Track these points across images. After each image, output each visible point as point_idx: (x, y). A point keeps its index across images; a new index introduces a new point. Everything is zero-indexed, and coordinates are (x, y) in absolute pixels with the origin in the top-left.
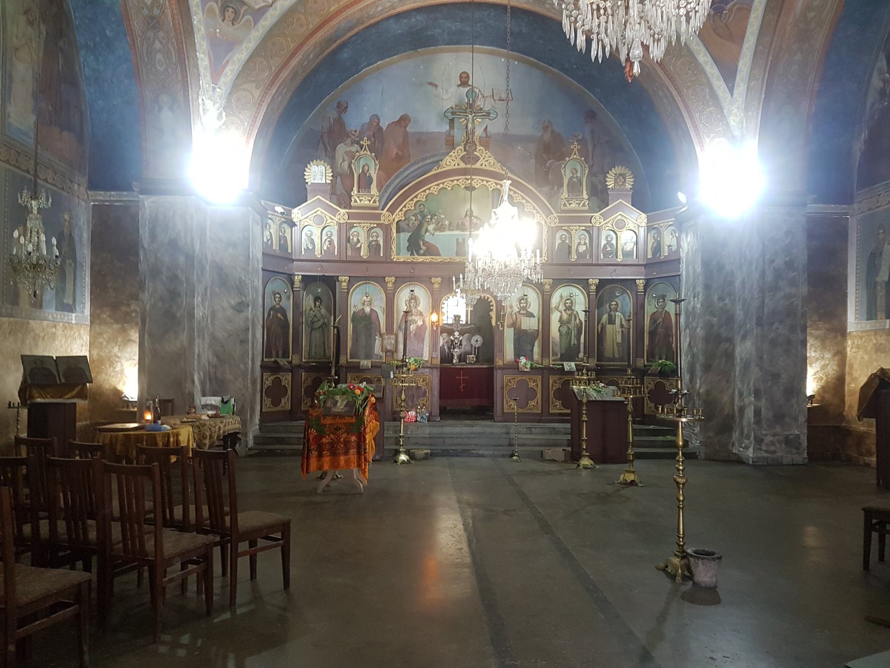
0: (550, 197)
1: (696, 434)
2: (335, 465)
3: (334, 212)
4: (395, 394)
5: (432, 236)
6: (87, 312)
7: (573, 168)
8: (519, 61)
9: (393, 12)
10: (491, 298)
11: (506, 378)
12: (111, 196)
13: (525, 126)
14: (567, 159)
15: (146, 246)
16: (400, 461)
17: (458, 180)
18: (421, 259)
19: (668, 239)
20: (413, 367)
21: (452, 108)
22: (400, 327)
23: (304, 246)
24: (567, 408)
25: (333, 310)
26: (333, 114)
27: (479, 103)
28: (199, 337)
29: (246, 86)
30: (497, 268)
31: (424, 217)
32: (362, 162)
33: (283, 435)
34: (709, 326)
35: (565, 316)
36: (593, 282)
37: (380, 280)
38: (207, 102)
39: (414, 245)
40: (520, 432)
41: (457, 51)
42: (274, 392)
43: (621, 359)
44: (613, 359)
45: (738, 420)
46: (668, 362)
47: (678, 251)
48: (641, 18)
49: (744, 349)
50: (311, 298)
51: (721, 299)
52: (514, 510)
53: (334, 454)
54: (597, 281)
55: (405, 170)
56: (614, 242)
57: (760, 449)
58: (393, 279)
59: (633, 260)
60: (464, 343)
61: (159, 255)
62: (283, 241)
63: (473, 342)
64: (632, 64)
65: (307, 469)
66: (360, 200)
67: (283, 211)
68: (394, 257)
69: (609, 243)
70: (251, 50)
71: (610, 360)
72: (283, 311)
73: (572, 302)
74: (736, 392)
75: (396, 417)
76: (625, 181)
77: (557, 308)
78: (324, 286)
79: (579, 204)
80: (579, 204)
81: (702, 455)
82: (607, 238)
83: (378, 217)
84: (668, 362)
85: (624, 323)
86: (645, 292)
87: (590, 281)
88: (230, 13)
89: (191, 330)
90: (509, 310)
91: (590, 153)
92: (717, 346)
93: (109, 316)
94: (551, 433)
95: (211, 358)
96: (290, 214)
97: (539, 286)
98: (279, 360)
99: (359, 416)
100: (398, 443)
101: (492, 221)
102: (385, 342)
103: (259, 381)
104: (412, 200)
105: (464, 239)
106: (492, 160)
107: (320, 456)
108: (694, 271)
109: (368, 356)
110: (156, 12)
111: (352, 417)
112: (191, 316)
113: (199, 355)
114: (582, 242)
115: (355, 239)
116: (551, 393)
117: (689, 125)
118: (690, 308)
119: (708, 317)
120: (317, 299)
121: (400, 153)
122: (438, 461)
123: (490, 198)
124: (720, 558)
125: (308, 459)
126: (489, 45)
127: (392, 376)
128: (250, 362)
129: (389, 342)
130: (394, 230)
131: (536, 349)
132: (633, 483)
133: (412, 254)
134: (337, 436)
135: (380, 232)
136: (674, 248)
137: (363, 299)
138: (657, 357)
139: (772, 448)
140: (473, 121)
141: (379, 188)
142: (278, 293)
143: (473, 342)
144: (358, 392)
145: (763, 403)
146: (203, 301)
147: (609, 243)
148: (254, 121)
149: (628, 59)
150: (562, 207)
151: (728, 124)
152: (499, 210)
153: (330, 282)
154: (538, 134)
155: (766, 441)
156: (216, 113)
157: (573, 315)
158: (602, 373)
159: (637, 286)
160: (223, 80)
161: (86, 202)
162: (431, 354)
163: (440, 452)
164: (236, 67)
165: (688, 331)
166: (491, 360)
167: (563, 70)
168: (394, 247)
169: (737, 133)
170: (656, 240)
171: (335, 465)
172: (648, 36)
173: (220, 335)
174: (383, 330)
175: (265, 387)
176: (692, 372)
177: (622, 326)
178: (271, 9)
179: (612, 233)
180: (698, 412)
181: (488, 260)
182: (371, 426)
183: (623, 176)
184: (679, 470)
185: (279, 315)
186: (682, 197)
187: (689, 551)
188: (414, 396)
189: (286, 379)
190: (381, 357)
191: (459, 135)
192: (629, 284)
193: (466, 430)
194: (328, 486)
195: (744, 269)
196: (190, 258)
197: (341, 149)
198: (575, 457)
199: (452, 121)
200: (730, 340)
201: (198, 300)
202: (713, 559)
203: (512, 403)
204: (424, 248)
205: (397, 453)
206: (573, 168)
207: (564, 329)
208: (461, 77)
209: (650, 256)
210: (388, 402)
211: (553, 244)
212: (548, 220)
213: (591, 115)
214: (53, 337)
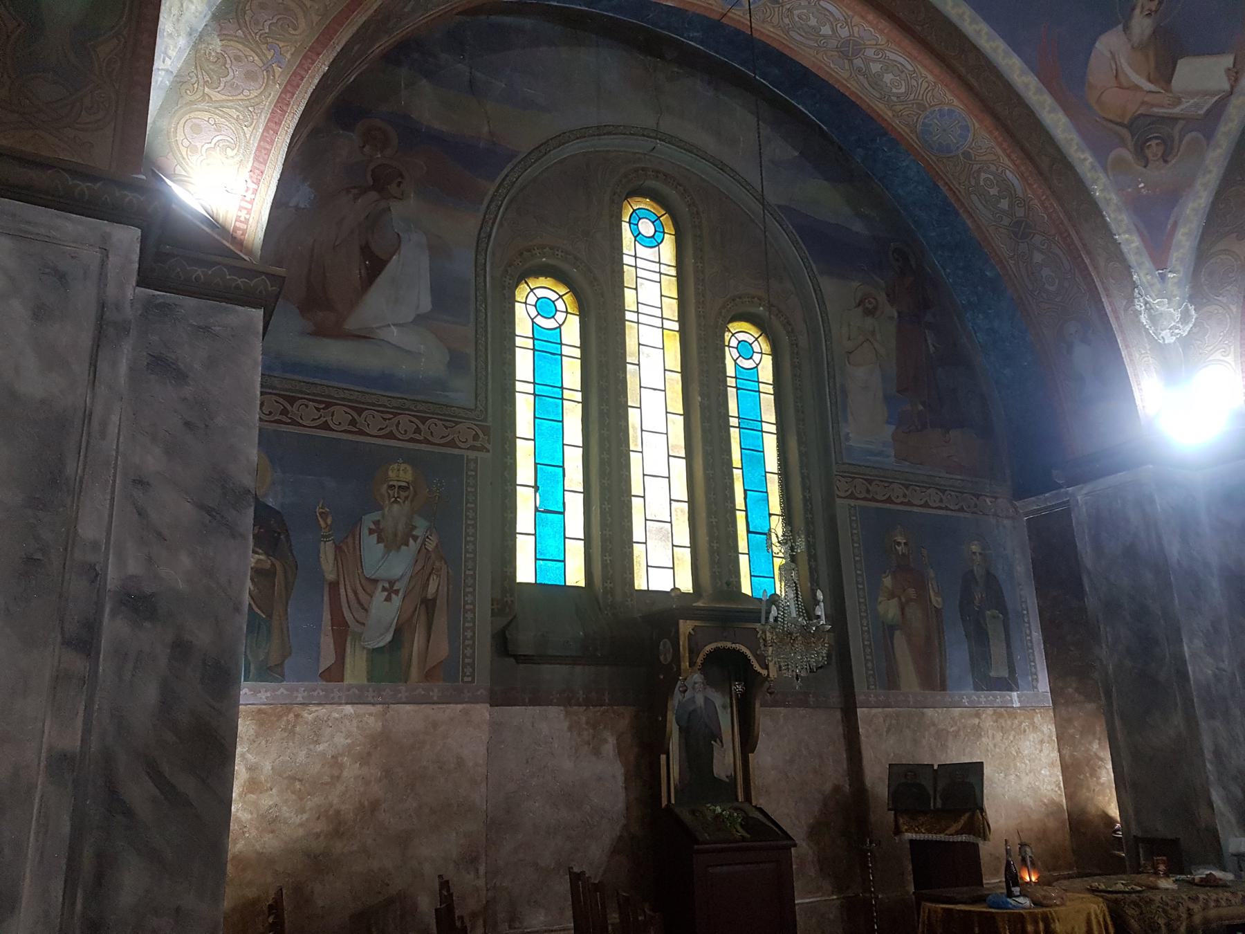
6: (1044, 685)
88: (1154, 148)
93: (1077, 690)
110: (1020, 213)
112: (1183, 676)
113: (1217, 753)
156: (1177, 315)
214: (977, 732)
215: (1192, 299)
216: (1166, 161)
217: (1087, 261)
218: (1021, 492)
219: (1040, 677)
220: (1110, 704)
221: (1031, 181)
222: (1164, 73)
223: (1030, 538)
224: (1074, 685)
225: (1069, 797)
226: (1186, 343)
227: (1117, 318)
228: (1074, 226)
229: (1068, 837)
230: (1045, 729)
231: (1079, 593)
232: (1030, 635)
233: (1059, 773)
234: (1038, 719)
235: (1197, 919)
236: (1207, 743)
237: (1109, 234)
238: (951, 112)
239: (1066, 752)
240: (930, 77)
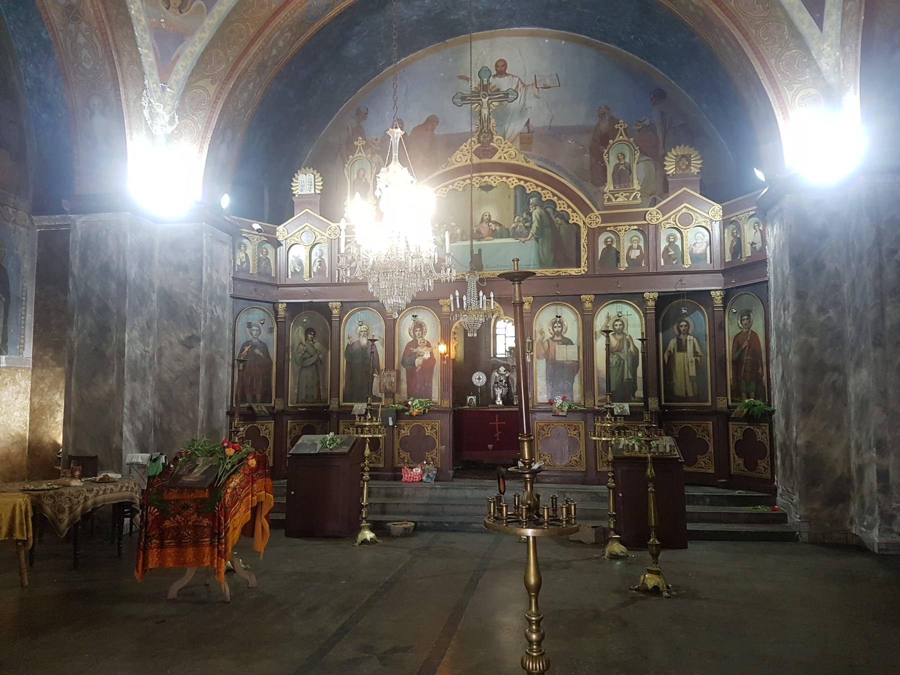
6: (28, 352)
8: (566, 40)
12: (56, 220)
14: (611, 141)
15: (76, 273)
19: (750, 235)
29: (201, 83)
34: (806, 351)
36: (651, 296)
41: (492, 36)
43: (697, 398)
44: (686, 399)
45: (856, 484)
47: (763, 250)
49: (859, 381)
51: (822, 310)
56: (678, 243)
57: (891, 531)
59: (707, 265)
61: (89, 283)
62: (262, 261)
67: (259, 227)
69: (671, 244)
70: (206, 42)
74: (853, 444)
80: (628, 197)
81: (805, 537)
82: (668, 239)
84: (758, 402)
85: (698, 350)
86: (725, 307)
89: (121, 372)
90: (539, 337)
92: (820, 377)
93: (52, 358)
95: (156, 404)
96: (274, 231)
98: (254, 406)
107: (162, 546)
108: (783, 274)
113: (133, 403)
114: (635, 246)
117: (762, 76)
118: (781, 325)
120: (308, 331)
126: (529, 26)
132: (656, 590)
136: (758, 246)
138: (744, 394)
140: (489, 105)
147: (671, 244)
148: (209, 122)
150: (606, 203)
151: (818, 70)
154: (593, 122)
156: (167, 118)
159: (712, 299)
160: (174, 78)
161: (28, 228)
164: (189, 62)
165: (780, 358)
167: (621, 44)
169: (832, 80)
170: (735, 237)
173: (166, 376)
174: (382, 365)
176: (787, 415)
177: (695, 353)
179: (675, 231)
183: (687, 157)
186: (759, 175)
192: (703, 297)
195: (853, 266)
196: (123, 284)
200: (838, 369)
207: (614, 360)
209: (728, 259)
213: (660, 95)
215: (178, 110)
216: (181, 12)
217: (115, 58)
218: (39, 209)
219: (26, 345)
220: (71, 370)
223: (39, 246)
224: (50, 354)
225: (32, 431)
227: (128, 106)
228: (105, 9)
229: (25, 458)
230: (23, 384)
231: (65, 290)
232: (25, 316)
233: (28, 415)
234: (18, 376)
235: (90, 502)
236: (127, 397)
237: (135, 45)
239: (36, 400)
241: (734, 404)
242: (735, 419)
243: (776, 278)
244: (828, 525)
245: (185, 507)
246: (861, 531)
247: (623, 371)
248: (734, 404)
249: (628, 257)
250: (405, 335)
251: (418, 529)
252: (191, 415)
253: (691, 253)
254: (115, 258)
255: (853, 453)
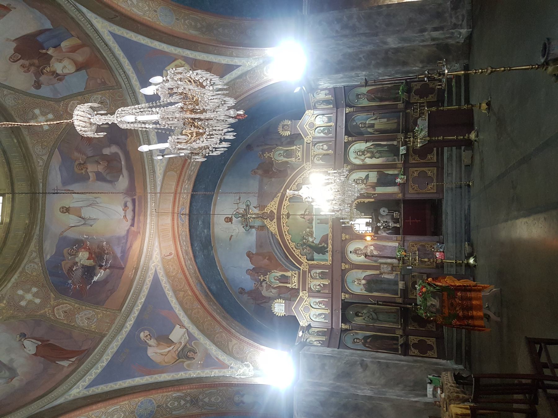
0: (294, 169)
1: (451, 67)
2: (480, 308)
3: (302, 299)
4: (424, 266)
5: (316, 238)
7: (278, 156)
9: (193, 259)
10: (356, 202)
11: (411, 191)
13: (254, 184)
16: (475, 263)
17: (283, 223)
18: (330, 246)
19: (322, 96)
20: (404, 253)
21: (243, 227)
22: (376, 261)
23: (323, 320)
24: (433, 150)
25: (364, 305)
26: (245, 297)
27: (241, 211)
28: (385, 395)
30: (339, 196)
31: (304, 244)
32: (273, 280)
33: (455, 343)
34: (377, 66)
35: (369, 155)
36: (346, 139)
37: (344, 273)
38: (238, 373)
39: (321, 250)
40: (451, 179)
41: (213, 224)
42: (423, 349)
43: (398, 118)
45: (441, 41)
46: (401, 88)
47: (329, 90)
48: (214, 111)
49: (392, 42)
50: (356, 319)
51: (360, 60)
52: (512, 182)
53: (471, 308)
54: (346, 136)
55: (277, 255)
56: (322, 128)
58: (343, 264)
59: (333, 116)
60: (385, 220)
62: (319, 333)
63: (384, 214)
64: (238, 115)
65: (482, 327)
66: (294, 283)
68: (329, 263)
69: (322, 131)
70: (211, 344)
71: (399, 125)
72: (366, 338)
73: (359, 151)
74: (421, 44)
75: (440, 266)
76: (287, 125)
77: (363, 160)
78: (348, 309)
79: (299, 151)
80: (299, 151)
83: (304, 272)
84: (401, 88)
86: (354, 107)
87: (346, 141)
88: (190, 354)
89: (380, 399)
91: (269, 146)
92: (388, 58)
94: (452, 161)
97: (350, 171)
98: (400, 344)
99: (443, 289)
100: (460, 265)
101: (310, 200)
102: (386, 271)
103: (415, 358)
104: (294, 251)
105: (318, 219)
106: (273, 203)
108: (342, 78)
109: (396, 283)
110: (188, 398)
111: (443, 295)
112: (370, 398)
113: (398, 396)
114: (321, 147)
115: (318, 287)
116: (422, 161)
119: (372, 67)
120: (357, 315)
121: (267, 258)
122: (473, 236)
123: (293, 203)
124: (548, 39)
125: (475, 326)
127: (411, 268)
128: (402, 363)
129: (385, 268)
130: (313, 262)
131: (391, 172)
132: (488, 104)
133: (327, 252)
134: (457, 304)
135: (313, 272)
136: (327, 92)
137: (356, 284)
138: (397, 95)
139: (460, 17)
141: (286, 271)
142: (354, 340)
143: (384, 214)
144: (424, 290)
145: (429, 27)
146: (360, 389)
147: (322, 131)
148: (250, 344)
149: (235, 118)
151: (256, 67)
152: (304, 196)
153: (346, 306)
154: (258, 177)
155: (455, 22)
156: (245, 368)
157: (368, 150)
158: (408, 129)
159: (350, 112)
162: (394, 241)
163: (467, 235)
164: (220, 353)
166: (397, 202)
167: (224, 164)
168: (322, 263)
171: (480, 308)
172: (223, 107)
173: (383, 381)
174: (377, 272)
175: (419, 354)
177: (376, 119)
178: (189, 330)
179: (316, 130)
180: (440, 63)
181: (334, 202)
182: (449, 281)
184: (482, 72)
185: (368, 340)
186: (297, 90)
187: (542, 60)
188: (424, 252)
189: (413, 339)
190: (397, 274)
191: (258, 223)
193: (449, 217)
194: (495, 314)
195: (341, 47)
196: (333, 394)
197: (265, 293)
198: (469, 144)
199: (251, 227)
200: (387, 51)
201: (360, 393)
202: (549, 44)
203: (429, 187)
204: (323, 244)
205: (468, 265)
206: (278, 156)
207: (377, 155)
208: (227, 222)
209: (332, 106)
210: (429, 271)
211: (320, 165)
212: (308, 169)
213: (249, 147)
215: (242, 362)
221: (181, 388)
222: (170, 343)
226: (256, 368)
238: (142, 403)
240: (126, 402)
241: (402, 100)
242: (409, 97)
243: (343, 82)
244: (460, 52)
245: (452, 305)
246: (462, 38)
247: (383, 151)
248: (402, 100)
249: (326, 150)
250: (360, 259)
251: (469, 240)
252: (405, 368)
253: (327, 123)
254: (317, 397)
255: (425, 43)
